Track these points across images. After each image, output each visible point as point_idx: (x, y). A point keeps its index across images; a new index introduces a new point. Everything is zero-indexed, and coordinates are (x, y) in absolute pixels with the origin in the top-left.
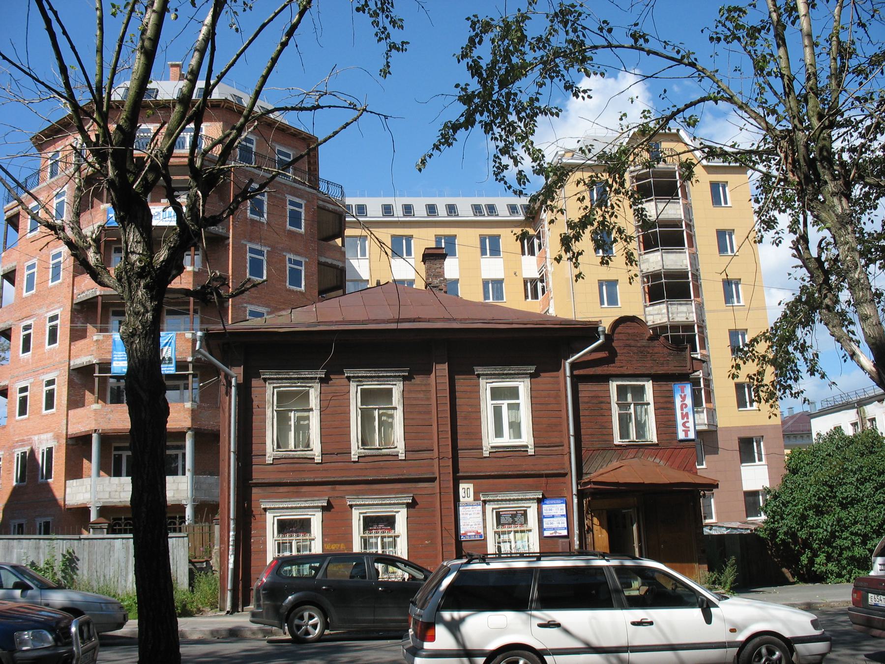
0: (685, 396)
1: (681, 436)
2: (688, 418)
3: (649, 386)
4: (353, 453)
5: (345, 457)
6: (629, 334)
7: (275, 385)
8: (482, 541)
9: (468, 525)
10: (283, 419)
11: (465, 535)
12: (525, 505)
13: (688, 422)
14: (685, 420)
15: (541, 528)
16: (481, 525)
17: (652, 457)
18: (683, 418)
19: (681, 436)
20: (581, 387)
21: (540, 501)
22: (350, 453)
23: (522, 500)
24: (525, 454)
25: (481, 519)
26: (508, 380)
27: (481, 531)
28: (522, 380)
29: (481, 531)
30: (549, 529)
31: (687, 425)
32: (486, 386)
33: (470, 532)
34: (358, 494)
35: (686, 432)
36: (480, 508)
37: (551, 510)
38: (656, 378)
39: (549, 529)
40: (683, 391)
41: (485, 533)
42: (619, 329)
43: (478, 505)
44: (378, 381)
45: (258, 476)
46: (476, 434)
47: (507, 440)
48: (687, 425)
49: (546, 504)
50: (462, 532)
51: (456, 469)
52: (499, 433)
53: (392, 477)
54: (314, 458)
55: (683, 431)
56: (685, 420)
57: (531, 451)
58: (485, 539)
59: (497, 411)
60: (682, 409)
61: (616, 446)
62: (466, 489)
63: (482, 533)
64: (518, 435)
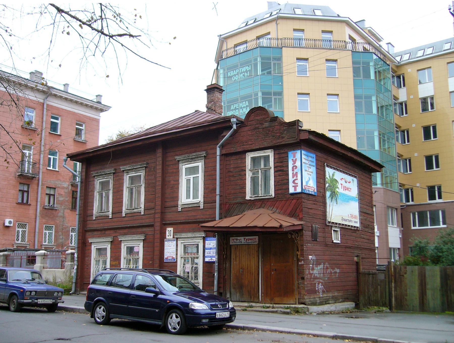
0: (296, 160)
1: (291, 190)
2: (297, 177)
3: (270, 153)
4: (123, 212)
5: (174, 209)
6: (258, 120)
7: (98, 179)
8: (174, 264)
9: (169, 253)
10: (101, 195)
11: (167, 259)
12: (197, 241)
13: (297, 179)
14: (295, 178)
15: (204, 257)
16: (175, 253)
17: (271, 207)
18: (293, 177)
19: (291, 190)
20: (54, 194)
21: (204, 239)
22: (122, 212)
23: (194, 237)
24: (139, 214)
25: (175, 250)
26: (193, 162)
27: (175, 256)
28: (200, 161)
29: (175, 256)
30: (208, 257)
31: (296, 182)
32: (184, 167)
33: (170, 257)
34: (125, 234)
35: (295, 187)
36: (175, 242)
37: (210, 244)
38: (274, 148)
39: (208, 257)
40: (294, 157)
41: (177, 258)
42: (252, 117)
43: (174, 241)
44: (135, 171)
45: (91, 226)
46: (176, 198)
47: (191, 200)
48: (296, 182)
49: (207, 240)
50: (165, 257)
51: (162, 219)
52: (188, 197)
53: (137, 225)
54: (109, 216)
55: (293, 186)
56: (295, 178)
57: (202, 207)
58: (176, 262)
59: (188, 181)
60: (293, 170)
61: (247, 200)
62: (170, 231)
63: (175, 258)
64: (195, 196)
